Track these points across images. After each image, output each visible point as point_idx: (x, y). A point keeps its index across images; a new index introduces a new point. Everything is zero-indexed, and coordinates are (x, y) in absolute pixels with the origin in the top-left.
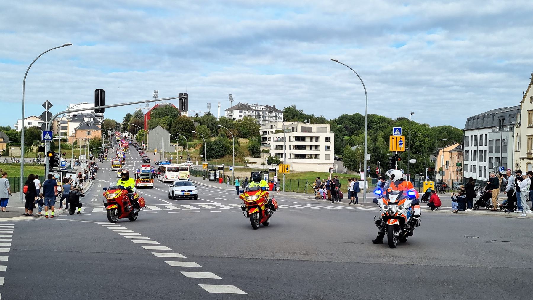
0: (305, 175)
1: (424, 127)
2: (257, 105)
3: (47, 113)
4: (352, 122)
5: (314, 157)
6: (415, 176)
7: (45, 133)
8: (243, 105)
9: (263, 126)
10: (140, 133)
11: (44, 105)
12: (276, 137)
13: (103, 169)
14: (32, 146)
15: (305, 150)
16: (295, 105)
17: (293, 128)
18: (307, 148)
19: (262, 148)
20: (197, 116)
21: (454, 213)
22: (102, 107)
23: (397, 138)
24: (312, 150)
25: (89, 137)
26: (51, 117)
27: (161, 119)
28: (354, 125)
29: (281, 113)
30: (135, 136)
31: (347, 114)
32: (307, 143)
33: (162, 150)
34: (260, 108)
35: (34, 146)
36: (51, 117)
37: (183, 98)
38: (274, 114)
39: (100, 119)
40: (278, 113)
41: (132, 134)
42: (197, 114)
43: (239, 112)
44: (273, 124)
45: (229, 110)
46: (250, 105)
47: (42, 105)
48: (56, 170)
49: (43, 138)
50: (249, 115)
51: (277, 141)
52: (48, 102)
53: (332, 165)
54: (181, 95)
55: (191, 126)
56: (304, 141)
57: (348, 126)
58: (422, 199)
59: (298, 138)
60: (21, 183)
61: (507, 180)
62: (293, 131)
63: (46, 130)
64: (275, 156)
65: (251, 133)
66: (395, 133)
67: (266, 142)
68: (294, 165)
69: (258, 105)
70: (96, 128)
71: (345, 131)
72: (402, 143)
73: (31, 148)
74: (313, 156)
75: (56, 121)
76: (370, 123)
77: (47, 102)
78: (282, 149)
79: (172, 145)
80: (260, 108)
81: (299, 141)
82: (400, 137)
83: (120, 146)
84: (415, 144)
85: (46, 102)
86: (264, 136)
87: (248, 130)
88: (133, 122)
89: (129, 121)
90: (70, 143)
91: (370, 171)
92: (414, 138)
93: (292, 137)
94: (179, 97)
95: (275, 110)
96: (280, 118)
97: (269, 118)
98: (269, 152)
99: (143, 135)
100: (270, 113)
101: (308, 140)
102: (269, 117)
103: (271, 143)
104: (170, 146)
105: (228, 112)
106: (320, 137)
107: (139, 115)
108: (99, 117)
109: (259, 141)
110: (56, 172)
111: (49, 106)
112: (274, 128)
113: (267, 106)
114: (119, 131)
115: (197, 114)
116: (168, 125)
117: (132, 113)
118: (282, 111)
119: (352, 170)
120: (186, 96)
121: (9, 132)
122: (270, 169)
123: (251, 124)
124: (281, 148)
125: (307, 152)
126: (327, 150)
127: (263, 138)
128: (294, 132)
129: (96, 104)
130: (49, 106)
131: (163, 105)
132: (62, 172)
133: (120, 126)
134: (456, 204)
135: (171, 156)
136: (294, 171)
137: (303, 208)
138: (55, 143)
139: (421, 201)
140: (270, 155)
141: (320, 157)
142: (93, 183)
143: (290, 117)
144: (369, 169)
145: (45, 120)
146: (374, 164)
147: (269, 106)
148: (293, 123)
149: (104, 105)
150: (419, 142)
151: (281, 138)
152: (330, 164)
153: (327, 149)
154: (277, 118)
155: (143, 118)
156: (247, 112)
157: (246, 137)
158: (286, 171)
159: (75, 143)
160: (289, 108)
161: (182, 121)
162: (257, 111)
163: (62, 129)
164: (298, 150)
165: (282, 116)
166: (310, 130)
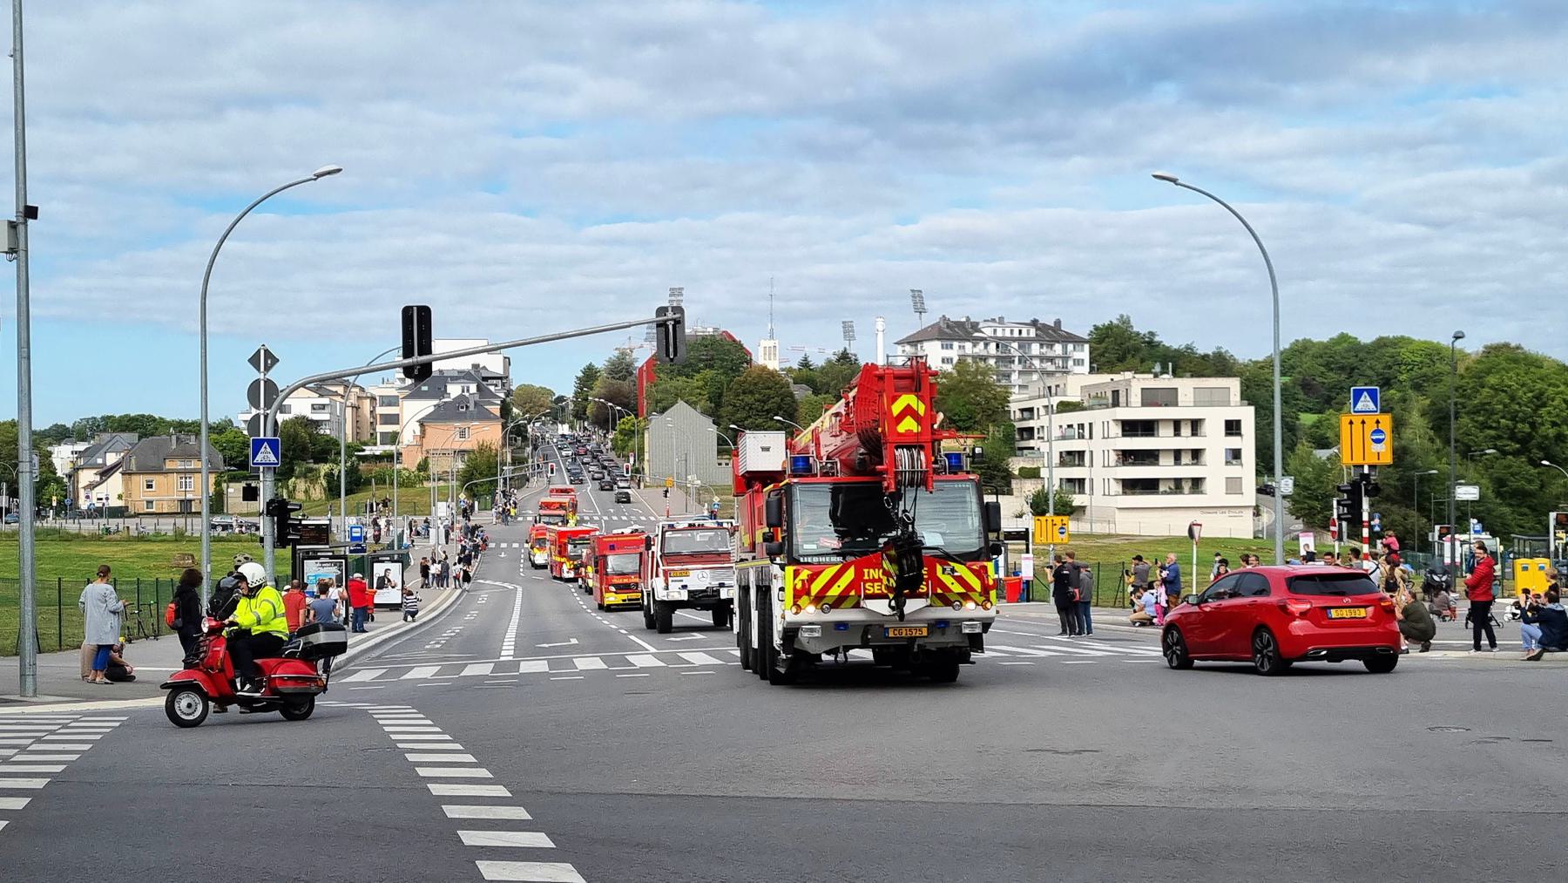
0: (1152, 548)
2: (1001, 319)
3: (262, 383)
4: (1327, 365)
5: (1187, 487)
6: (1516, 541)
7: (258, 445)
8: (955, 323)
9: (1021, 391)
10: (623, 426)
11: (254, 360)
12: (1061, 427)
13: (504, 545)
14: (293, 479)
15: (1158, 464)
16: (1128, 317)
17: (1116, 393)
18: (1162, 461)
19: (1016, 464)
20: (805, 364)
21: (1529, 659)
22: (425, 358)
23: (1363, 422)
24: (1180, 464)
25: (467, 446)
26: (275, 397)
27: (689, 380)
28: (1333, 377)
29: (1083, 346)
30: (610, 436)
31: (1308, 338)
32: (1163, 440)
33: (694, 481)
34: (1012, 331)
35: (298, 481)
36: (275, 397)
37: (668, 323)
38: (1058, 349)
39: (496, 385)
40: (1070, 347)
41: (600, 431)
42: (806, 359)
43: (943, 348)
44: (1052, 382)
45: (909, 343)
46: (978, 324)
47: (249, 360)
48: (331, 554)
49: (254, 459)
50: (974, 357)
51: (1064, 438)
52: (266, 351)
53: (1251, 511)
54: (661, 311)
55: (782, 400)
56: (1153, 435)
57: (1314, 379)
58: (1467, 619)
60: (205, 597)
61: (118, 588)
62: (1116, 404)
63: (262, 437)
64: (1056, 487)
65: (979, 416)
66: (1360, 406)
67: (1032, 443)
68: (1119, 516)
69: (1006, 321)
70: (486, 416)
71: (1299, 397)
72: (1381, 437)
73: (291, 488)
74: (1183, 483)
75: (368, 397)
76: (1390, 368)
77: (262, 352)
78: (1081, 464)
79: (723, 462)
80: (1012, 331)
81: (1137, 435)
82: (1360, 419)
83: (552, 472)
84: (1537, 432)
85: (259, 351)
86: (1024, 422)
87: (970, 404)
88: (602, 391)
89: (591, 389)
90: (406, 466)
91: (1382, 530)
92: (1535, 411)
93: (1111, 423)
94: (658, 319)
95: (1061, 336)
96: (1079, 362)
97: (1042, 361)
98: (1039, 477)
99: (633, 432)
100: (1045, 348)
102: (1042, 358)
103: (1044, 447)
104: (720, 464)
105: (908, 348)
107: (621, 368)
108: (495, 382)
109: (1008, 439)
110: (327, 560)
111: (269, 362)
112: (1056, 394)
113: (1034, 323)
114: (563, 423)
115: (806, 359)
116: (710, 399)
117: (600, 363)
118: (1087, 338)
119: (1320, 527)
120: (677, 316)
121: (223, 438)
122: (1010, 533)
123: (978, 386)
124: (1077, 462)
125: (1164, 470)
126: (1232, 464)
127: (1022, 430)
128: (1117, 409)
129: (407, 352)
130: (269, 362)
131: (693, 333)
132: (343, 561)
133: (567, 405)
134: (1535, 630)
135: (716, 499)
136: (1117, 536)
137: (1108, 653)
138: (360, 468)
139: (1467, 623)
140: (1043, 486)
141: (1207, 486)
142: (464, 591)
143: (1113, 357)
144: (1377, 521)
145: (258, 407)
146: (1393, 504)
147: (1041, 322)
148: (1116, 377)
149: (430, 352)
150: (1554, 424)
151: (1076, 427)
153: (1230, 459)
154: (1070, 363)
155: (632, 378)
156: (968, 345)
157: (967, 429)
158: (1058, 538)
159: (423, 467)
160: (1110, 327)
161: (755, 384)
162: (1001, 343)
163: (386, 423)
164: (1133, 464)
165: (1084, 354)
166: (1170, 398)
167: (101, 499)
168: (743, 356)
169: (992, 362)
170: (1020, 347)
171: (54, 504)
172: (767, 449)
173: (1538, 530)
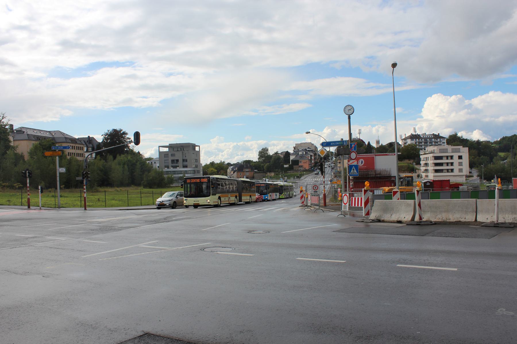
5: (450, 171)
32: (444, 161)
38: (439, 140)
40: (442, 139)
59: (436, 158)
96: (443, 143)
106: (453, 156)
141: (454, 171)
152: (463, 176)
167: (437, 302)
168: (475, 130)
169: (423, 143)
170: (429, 140)
171: (296, 177)
172: (194, 154)
173: (126, 141)
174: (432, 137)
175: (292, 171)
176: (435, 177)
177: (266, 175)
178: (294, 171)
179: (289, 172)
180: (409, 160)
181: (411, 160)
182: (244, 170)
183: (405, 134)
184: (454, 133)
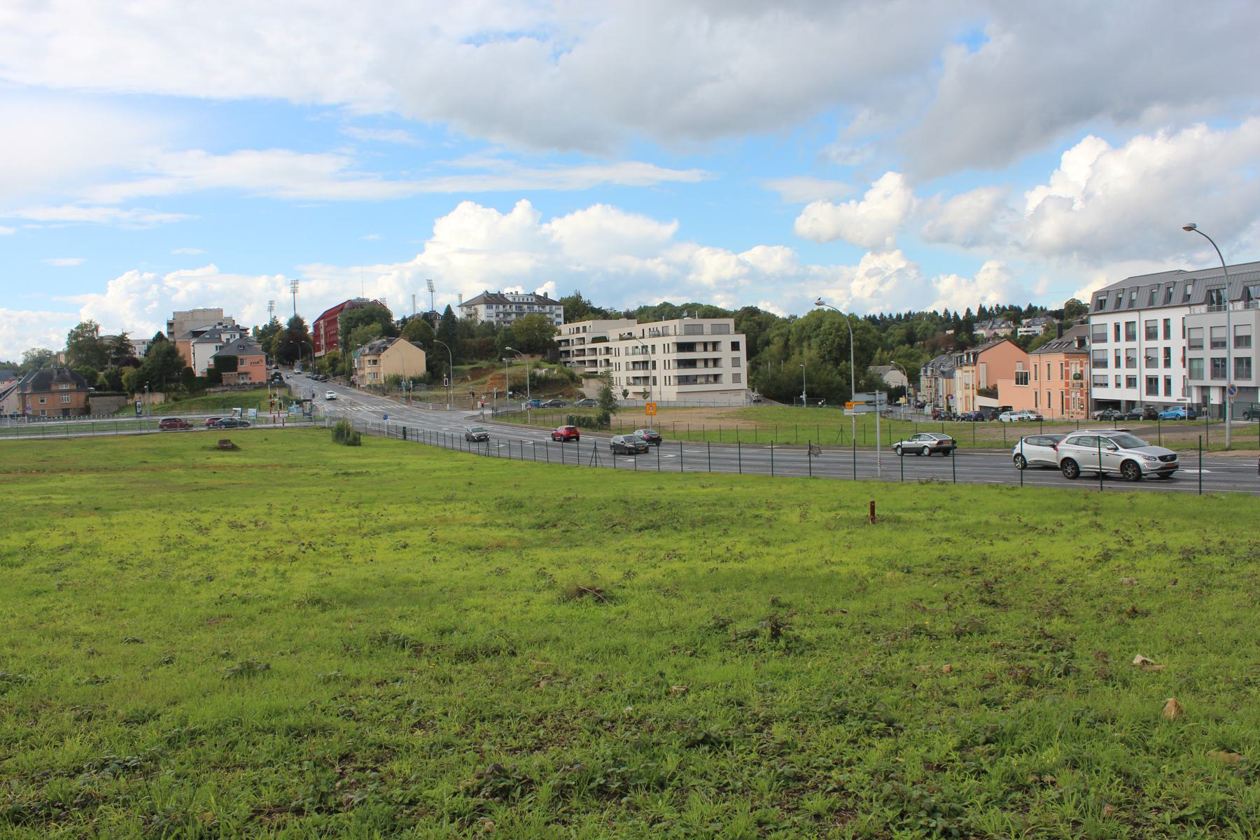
1: (853, 318)
5: (711, 379)
38: (547, 308)
40: (554, 307)
56: (693, 351)
59: (682, 347)
96: (558, 316)
101: (700, 348)
125: (700, 370)
156: (501, 307)
169: (514, 316)
174: (534, 301)
175: (221, 389)
176: (681, 395)
177: (130, 402)
178: (225, 388)
179: (212, 390)
180: (532, 357)
181: (537, 356)
182: (54, 388)
183: (460, 296)
184: (572, 294)
